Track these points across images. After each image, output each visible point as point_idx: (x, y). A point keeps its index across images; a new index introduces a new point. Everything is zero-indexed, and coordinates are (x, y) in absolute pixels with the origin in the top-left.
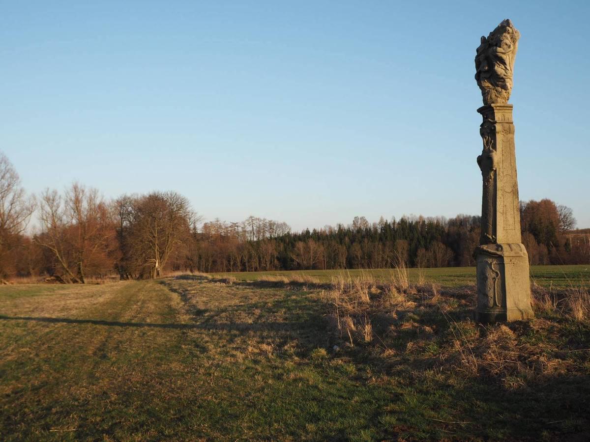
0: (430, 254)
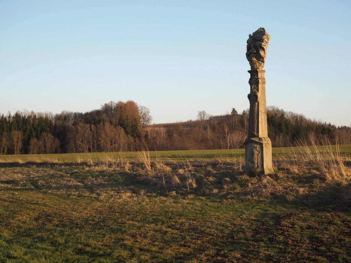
0: (41, 143)
